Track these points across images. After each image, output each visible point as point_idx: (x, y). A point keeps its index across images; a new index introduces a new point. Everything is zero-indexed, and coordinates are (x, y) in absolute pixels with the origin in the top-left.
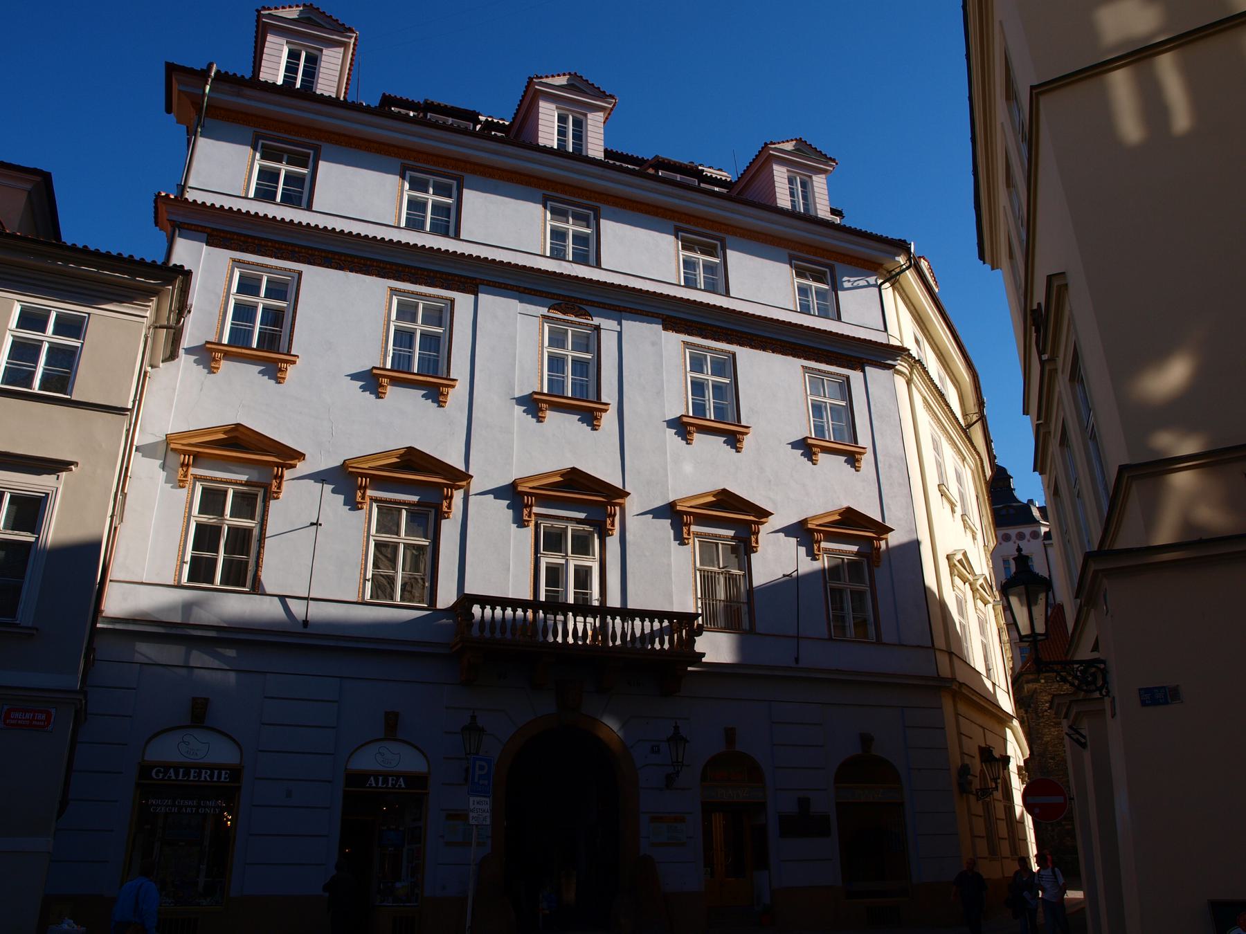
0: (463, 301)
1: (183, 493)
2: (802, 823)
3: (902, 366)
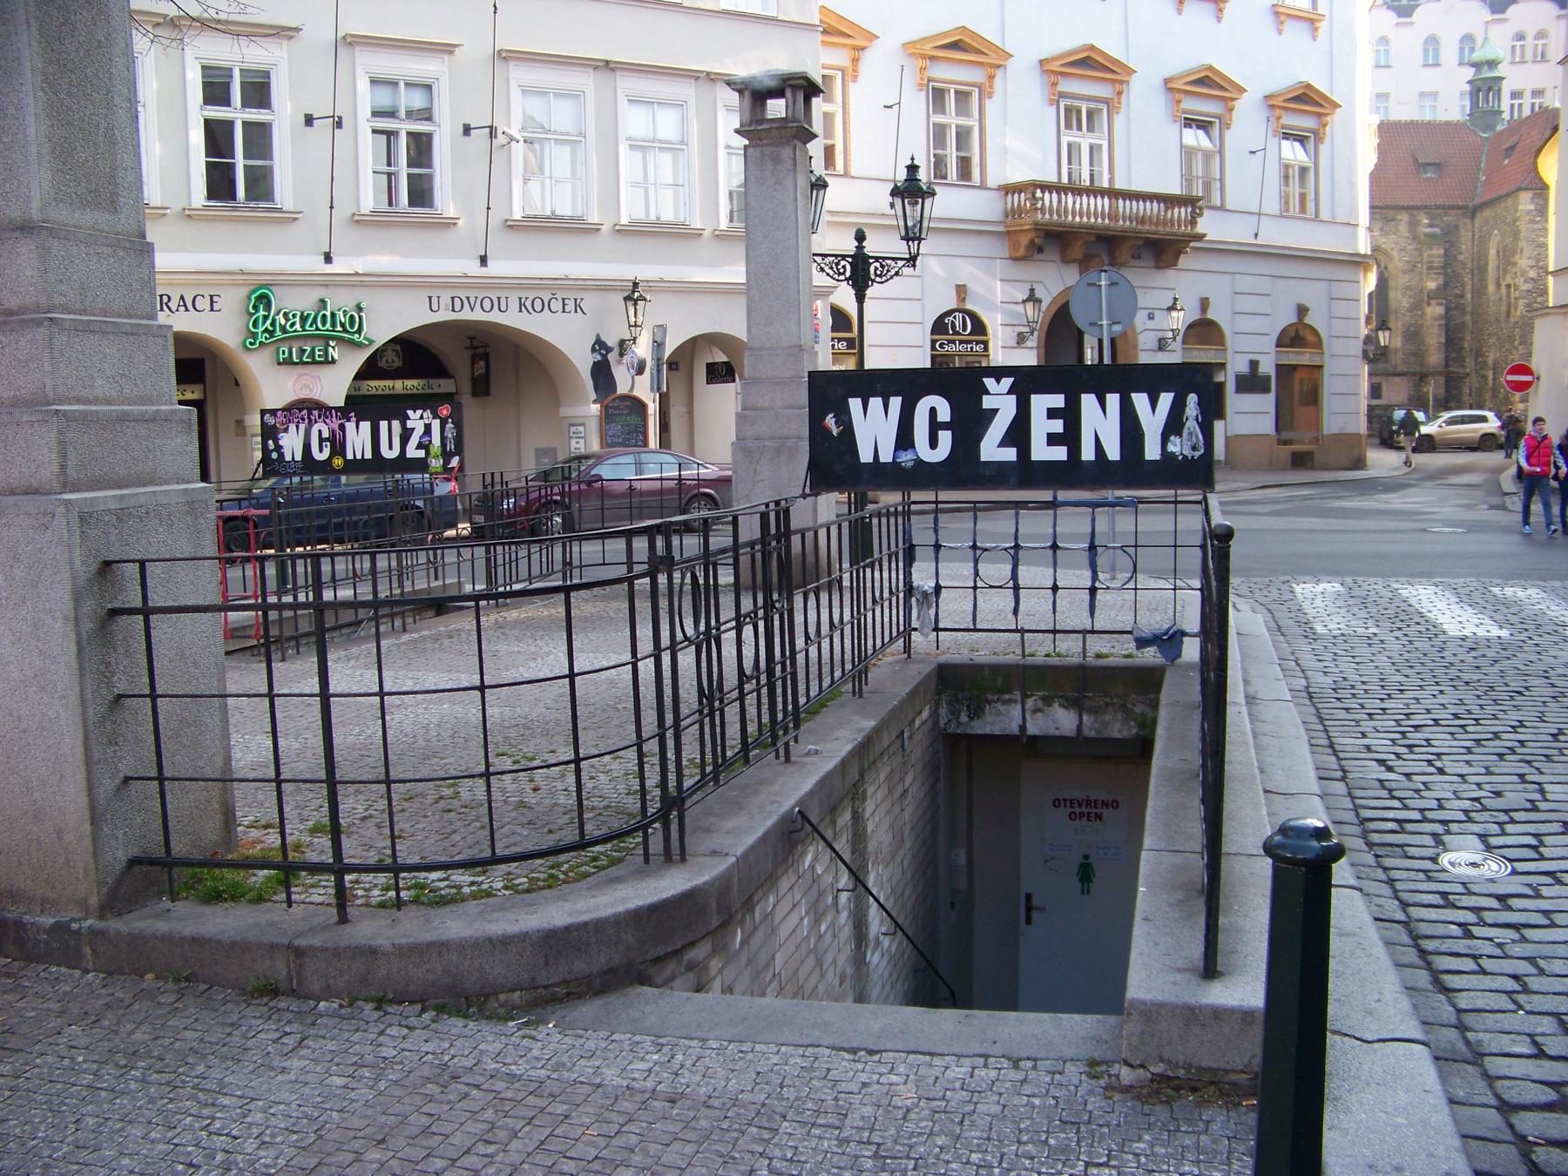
2: (1251, 382)
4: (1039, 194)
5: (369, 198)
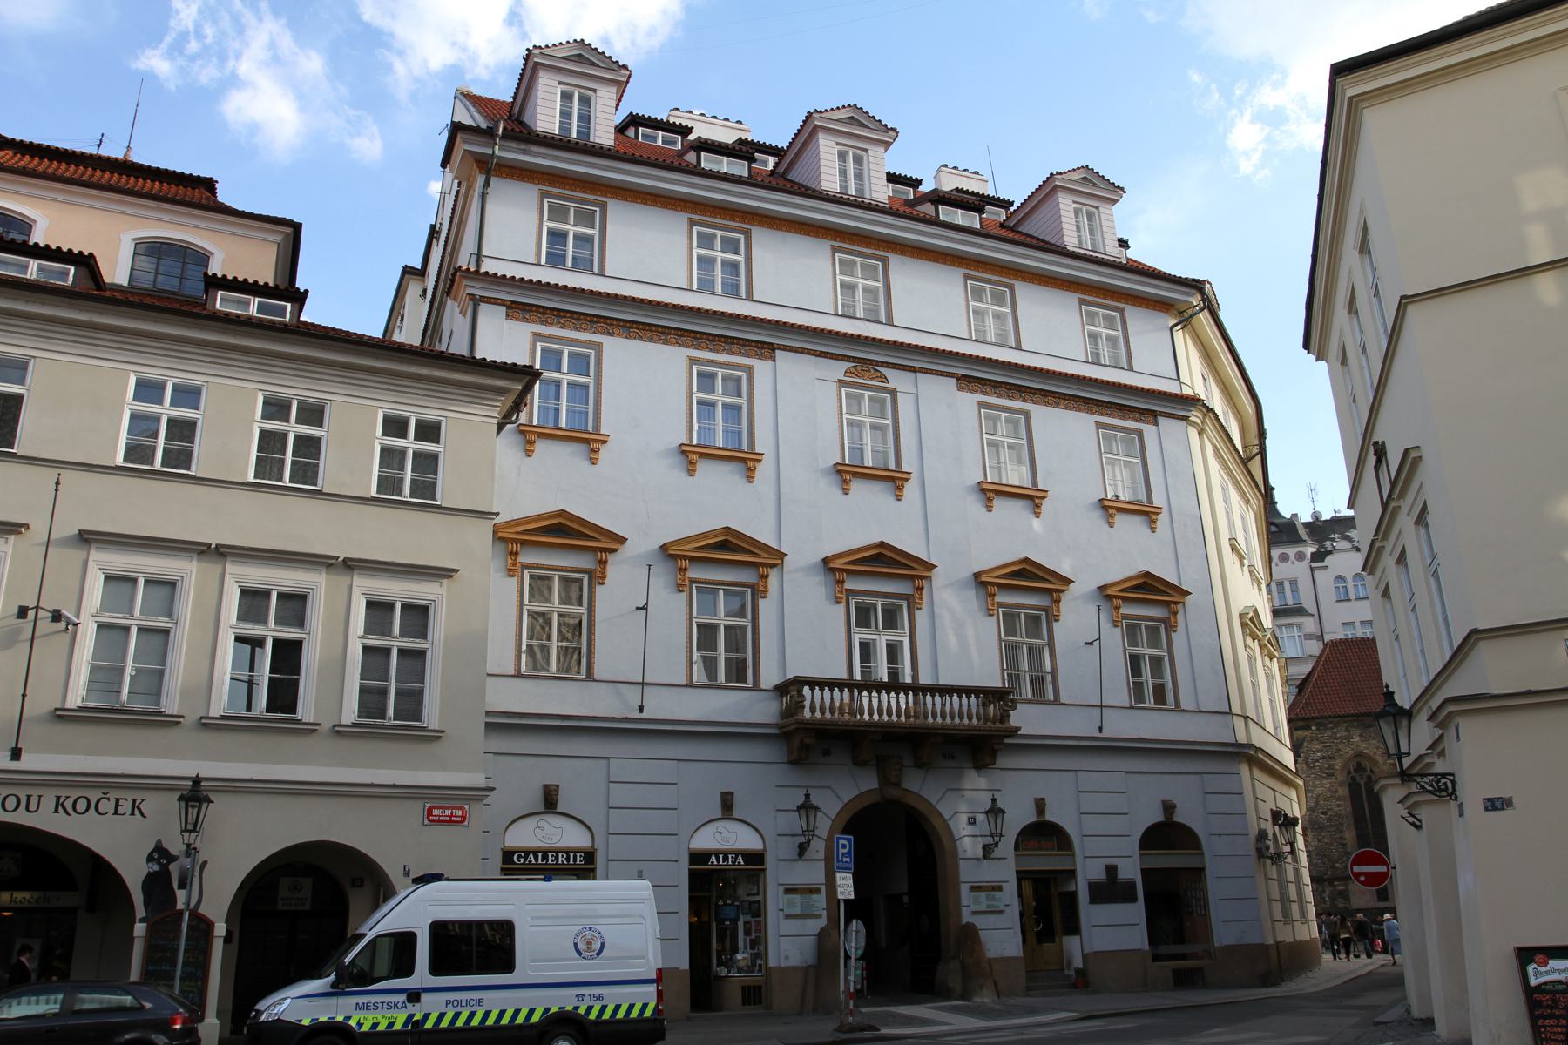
0: (761, 367)
1: (514, 581)
2: (1110, 890)
3: (1196, 416)
4: (806, 690)
5: (350, 712)
